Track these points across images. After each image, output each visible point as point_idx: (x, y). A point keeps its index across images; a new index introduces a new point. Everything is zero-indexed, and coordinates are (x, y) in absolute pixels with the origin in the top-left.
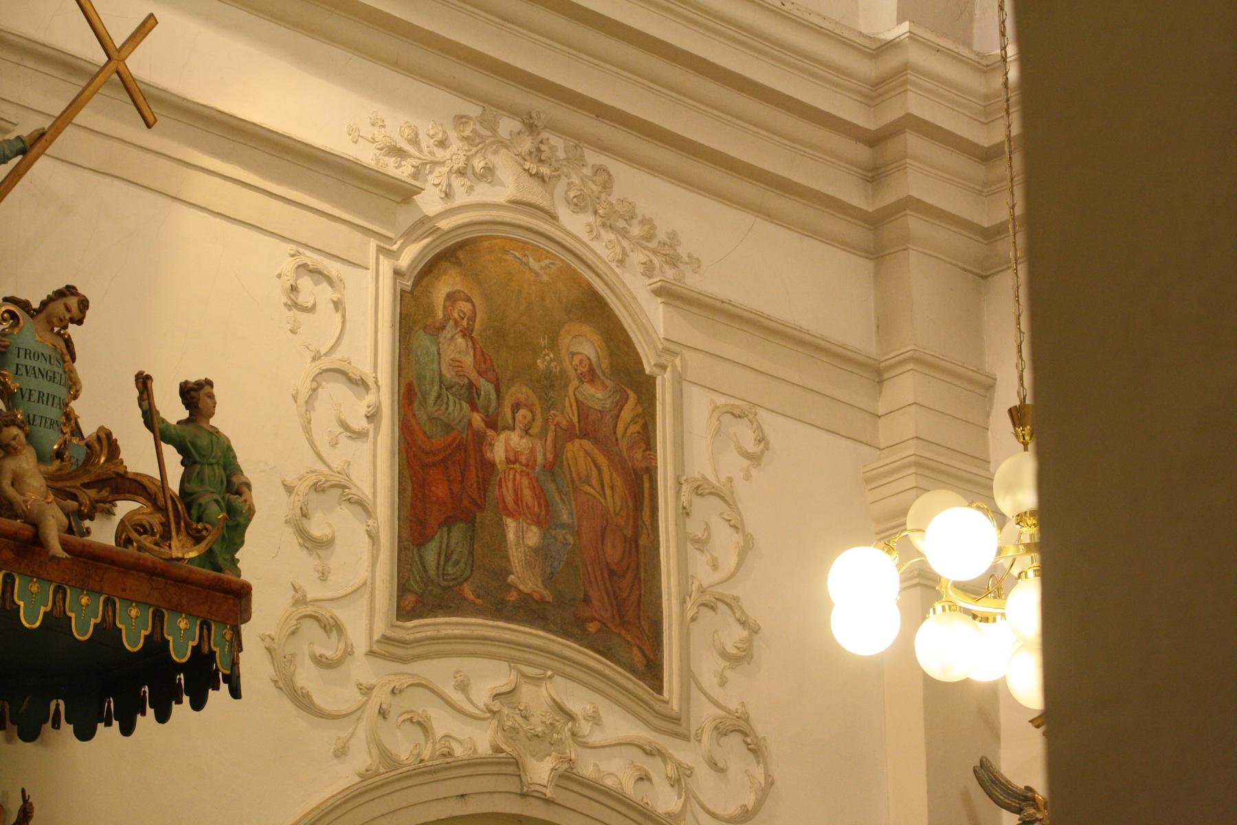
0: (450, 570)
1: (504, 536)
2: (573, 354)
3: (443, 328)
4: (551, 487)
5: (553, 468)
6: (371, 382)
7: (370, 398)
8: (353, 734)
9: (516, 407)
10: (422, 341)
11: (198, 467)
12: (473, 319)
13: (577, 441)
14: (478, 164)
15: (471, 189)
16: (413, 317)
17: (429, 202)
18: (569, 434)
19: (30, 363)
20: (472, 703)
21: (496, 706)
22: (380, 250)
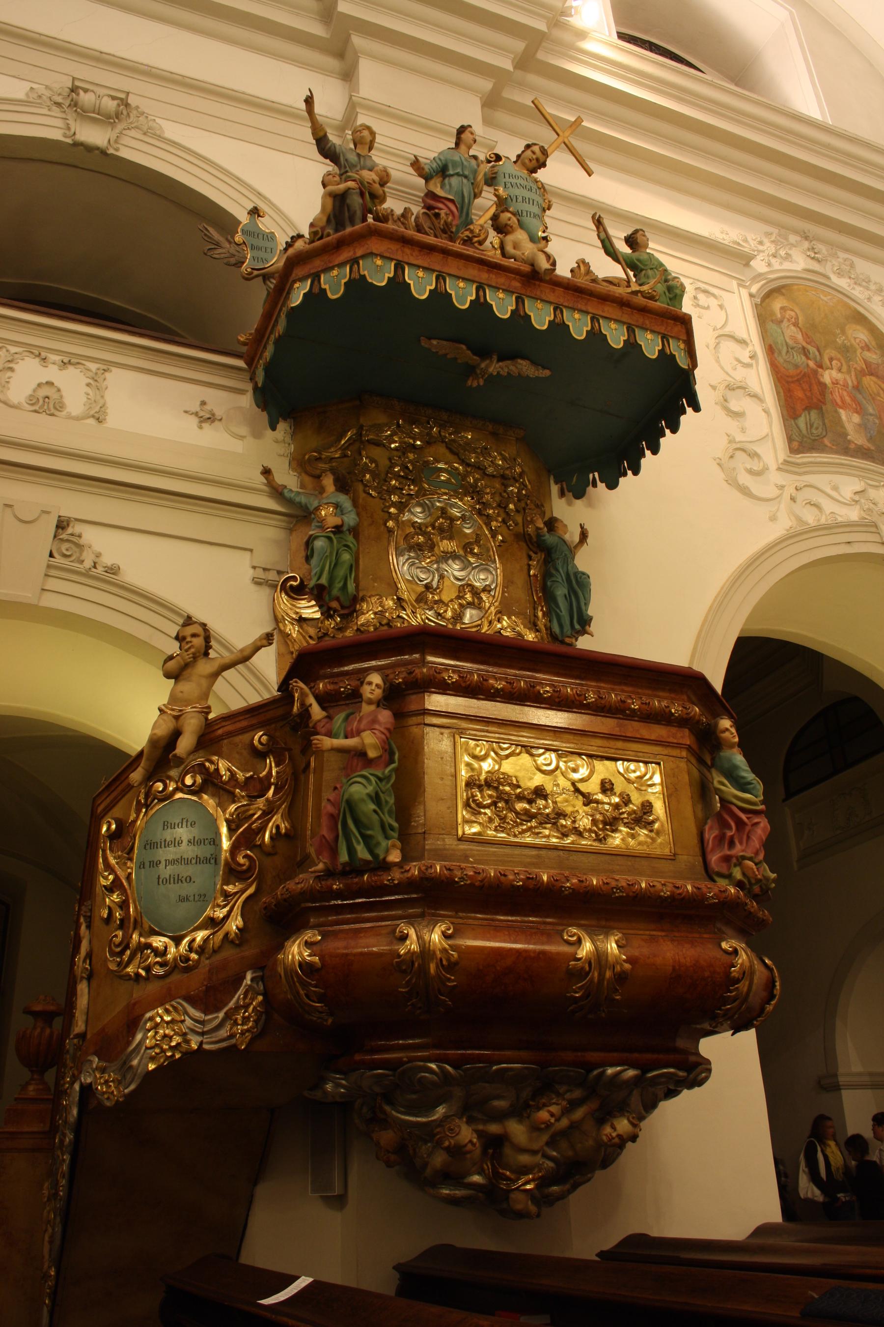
0: (814, 431)
1: (840, 417)
2: (855, 338)
3: (782, 321)
4: (859, 396)
5: (857, 387)
6: (749, 341)
7: (750, 348)
8: (778, 510)
9: (831, 360)
10: (771, 326)
11: (644, 272)
12: (797, 318)
13: (868, 377)
14: (782, 253)
15: (781, 263)
16: (763, 316)
17: (759, 265)
18: (861, 373)
19: (514, 181)
20: (841, 496)
21: (857, 498)
22: (739, 285)
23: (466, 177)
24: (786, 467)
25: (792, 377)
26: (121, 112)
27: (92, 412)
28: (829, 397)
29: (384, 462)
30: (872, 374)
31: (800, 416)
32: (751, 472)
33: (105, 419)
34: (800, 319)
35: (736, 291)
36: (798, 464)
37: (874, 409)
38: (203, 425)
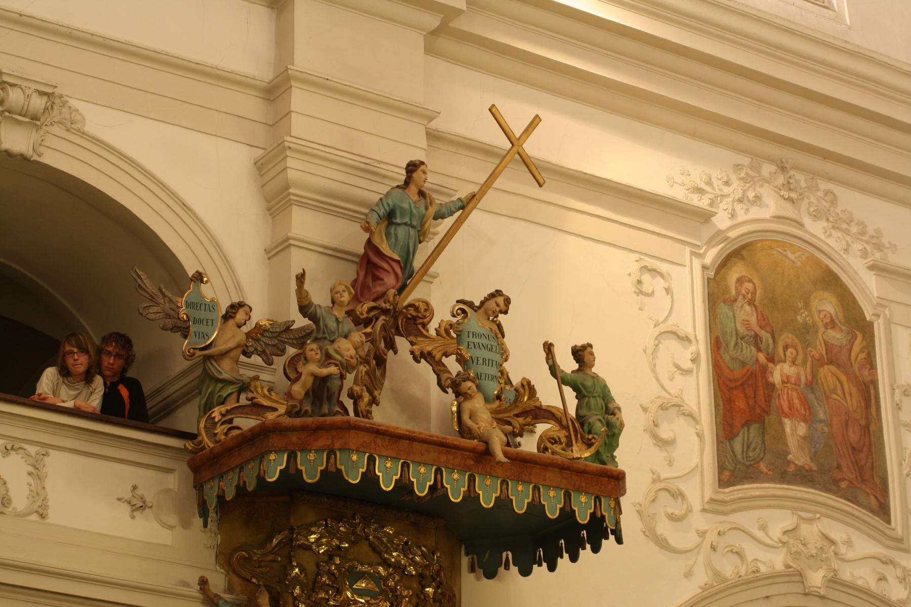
0: (751, 454)
2: (820, 311)
3: (736, 300)
4: (811, 397)
5: (812, 385)
7: (692, 348)
9: (786, 348)
10: (723, 309)
11: (586, 399)
12: (754, 293)
14: (751, 195)
16: (716, 295)
17: (722, 221)
18: (820, 362)
19: (476, 340)
20: (769, 536)
21: (785, 539)
22: (693, 253)
23: (413, 227)
24: (714, 507)
25: (736, 380)
26: (47, 111)
27: (35, 507)
28: (775, 402)
29: (312, 568)
30: (831, 362)
31: (738, 435)
32: (672, 518)
33: (47, 514)
34: (758, 292)
35: (688, 263)
36: (725, 502)
37: (825, 413)
38: (135, 513)
